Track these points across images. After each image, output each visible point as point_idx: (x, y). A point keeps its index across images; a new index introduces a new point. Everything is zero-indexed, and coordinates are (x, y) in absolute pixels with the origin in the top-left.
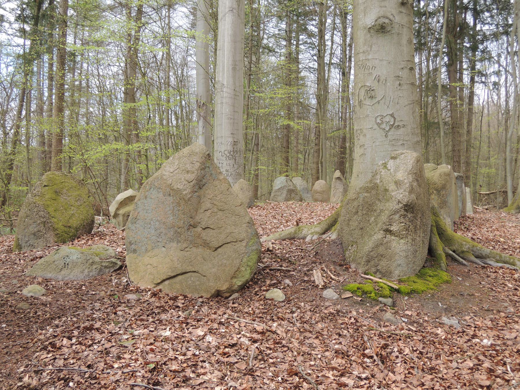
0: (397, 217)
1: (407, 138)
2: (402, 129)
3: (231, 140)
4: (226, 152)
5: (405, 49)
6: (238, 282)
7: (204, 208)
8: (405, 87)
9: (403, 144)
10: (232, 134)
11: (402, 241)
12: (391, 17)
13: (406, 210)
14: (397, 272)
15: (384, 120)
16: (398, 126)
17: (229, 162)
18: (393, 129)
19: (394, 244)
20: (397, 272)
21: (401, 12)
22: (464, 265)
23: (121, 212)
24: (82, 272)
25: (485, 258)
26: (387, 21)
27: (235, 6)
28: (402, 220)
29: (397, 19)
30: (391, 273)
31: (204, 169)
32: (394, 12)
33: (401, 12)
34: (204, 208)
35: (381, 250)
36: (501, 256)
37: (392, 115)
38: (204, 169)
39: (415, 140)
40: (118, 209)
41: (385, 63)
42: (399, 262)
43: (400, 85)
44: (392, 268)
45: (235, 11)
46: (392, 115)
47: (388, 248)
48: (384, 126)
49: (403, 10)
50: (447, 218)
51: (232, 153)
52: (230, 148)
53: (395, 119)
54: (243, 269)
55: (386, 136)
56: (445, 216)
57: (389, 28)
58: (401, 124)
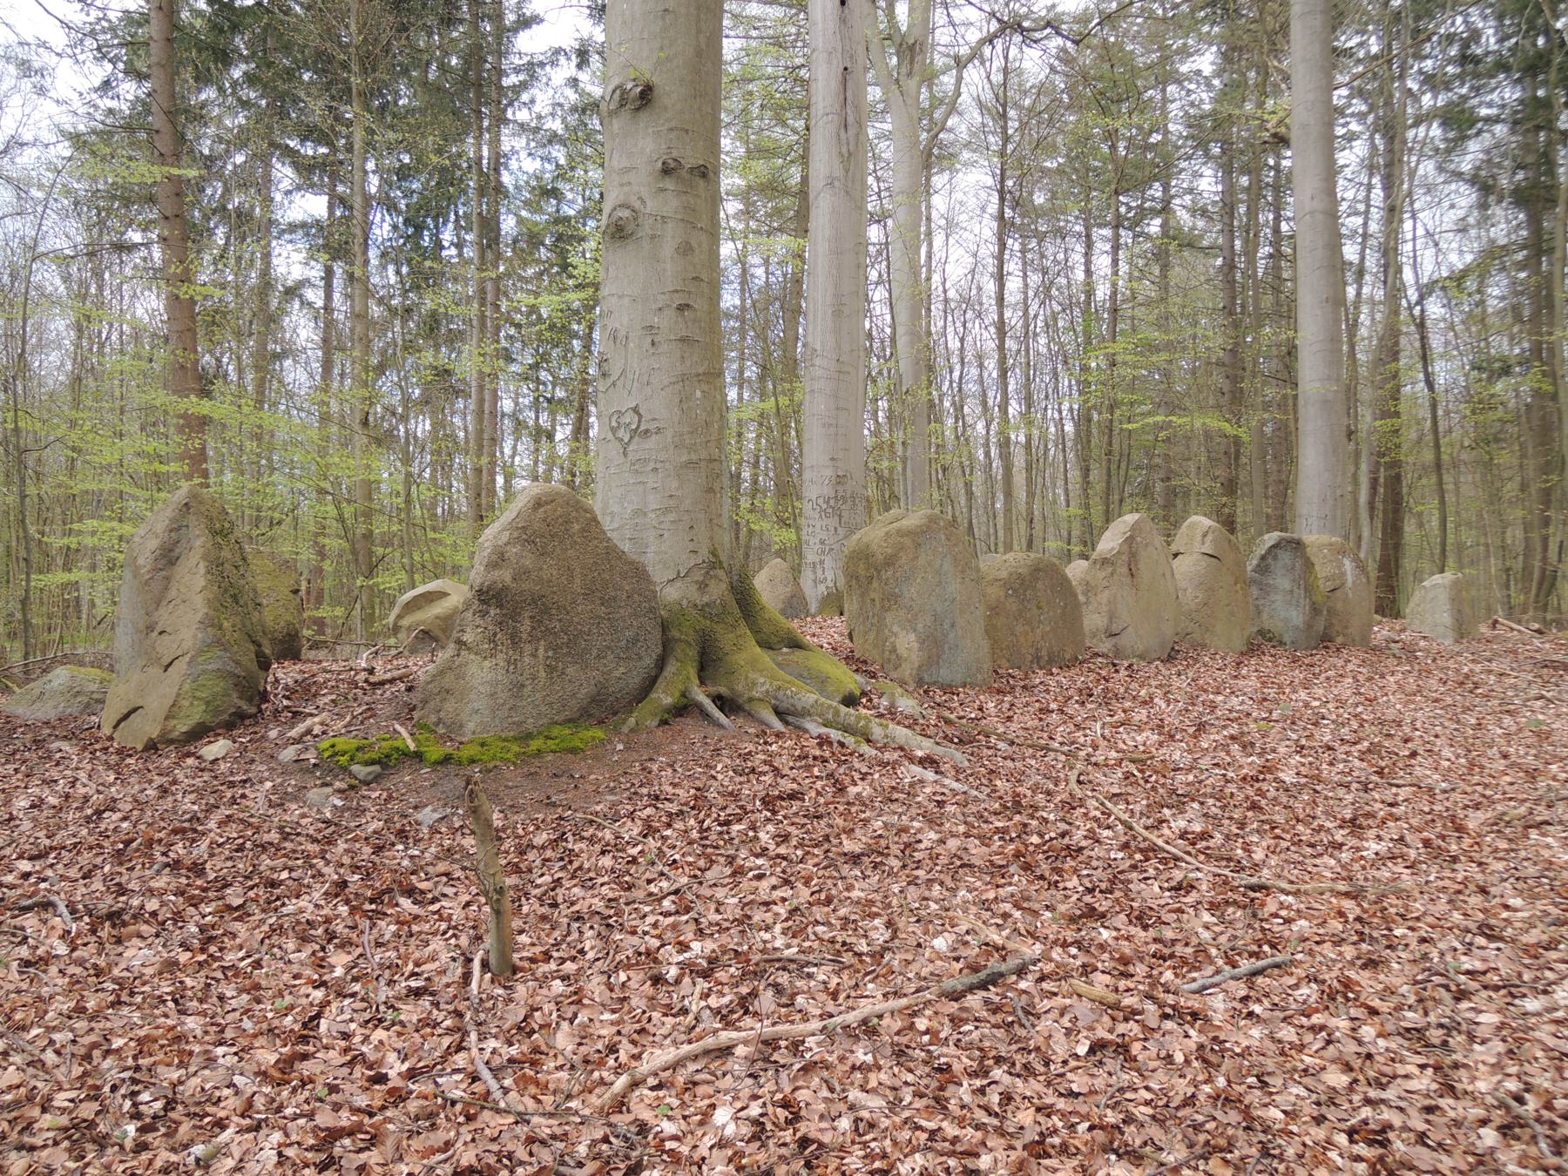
0: (469, 615)
1: (662, 456)
2: (654, 437)
3: (829, 472)
4: (821, 501)
5: (668, 267)
6: (182, 727)
7: (170, 597)
8: (664, 348)
9: (655, 470)
10: (832, 459)
11: (487, 663)
12: (637, 205)
13: (483, 602)
14: (471, 726)
15: (622, 420)
16: (647, 431)
17: (826, 522)
18: (636, 439)
19: (473, 669)
20: (471, 726)
21: (663, 190)
22: (721, 726)
23: (405, 622)
24: (56, 707)
25: (803, 716)
26: (625, 213)
27: (838, 172)
28: (479, 621)
29: (651, 206)
30: (461, 726)
31: (178, 529)
32: (644, 192)
33: (663, 190)
34: (170, 597)
35: (450, 677)
36: (837, 713)
37: (635, 410)
38: (178, 529)
39: (684, 458)
40: (400, 617)
41: (626, 300)
42: (476, 705)
43: (653, 344)
44: (464, 717)
45: (837, 184)
46: (635, 410)
47: (460, 677)
48: (621, 433)
49: (669, 184)
50: (902, 634)
51: (832, 502)
52: (828, 491)
53: (640, 416)
54: (186, 703)
55: (625, 454)
56: (895, 629)
57: (630, 228)
58: (652, 426)
